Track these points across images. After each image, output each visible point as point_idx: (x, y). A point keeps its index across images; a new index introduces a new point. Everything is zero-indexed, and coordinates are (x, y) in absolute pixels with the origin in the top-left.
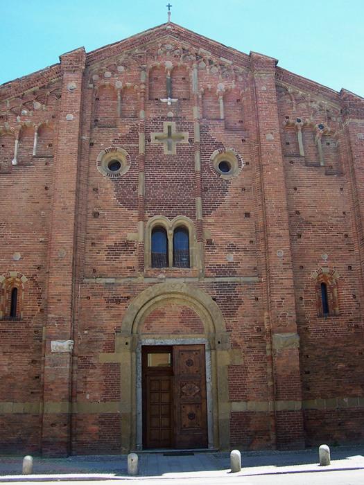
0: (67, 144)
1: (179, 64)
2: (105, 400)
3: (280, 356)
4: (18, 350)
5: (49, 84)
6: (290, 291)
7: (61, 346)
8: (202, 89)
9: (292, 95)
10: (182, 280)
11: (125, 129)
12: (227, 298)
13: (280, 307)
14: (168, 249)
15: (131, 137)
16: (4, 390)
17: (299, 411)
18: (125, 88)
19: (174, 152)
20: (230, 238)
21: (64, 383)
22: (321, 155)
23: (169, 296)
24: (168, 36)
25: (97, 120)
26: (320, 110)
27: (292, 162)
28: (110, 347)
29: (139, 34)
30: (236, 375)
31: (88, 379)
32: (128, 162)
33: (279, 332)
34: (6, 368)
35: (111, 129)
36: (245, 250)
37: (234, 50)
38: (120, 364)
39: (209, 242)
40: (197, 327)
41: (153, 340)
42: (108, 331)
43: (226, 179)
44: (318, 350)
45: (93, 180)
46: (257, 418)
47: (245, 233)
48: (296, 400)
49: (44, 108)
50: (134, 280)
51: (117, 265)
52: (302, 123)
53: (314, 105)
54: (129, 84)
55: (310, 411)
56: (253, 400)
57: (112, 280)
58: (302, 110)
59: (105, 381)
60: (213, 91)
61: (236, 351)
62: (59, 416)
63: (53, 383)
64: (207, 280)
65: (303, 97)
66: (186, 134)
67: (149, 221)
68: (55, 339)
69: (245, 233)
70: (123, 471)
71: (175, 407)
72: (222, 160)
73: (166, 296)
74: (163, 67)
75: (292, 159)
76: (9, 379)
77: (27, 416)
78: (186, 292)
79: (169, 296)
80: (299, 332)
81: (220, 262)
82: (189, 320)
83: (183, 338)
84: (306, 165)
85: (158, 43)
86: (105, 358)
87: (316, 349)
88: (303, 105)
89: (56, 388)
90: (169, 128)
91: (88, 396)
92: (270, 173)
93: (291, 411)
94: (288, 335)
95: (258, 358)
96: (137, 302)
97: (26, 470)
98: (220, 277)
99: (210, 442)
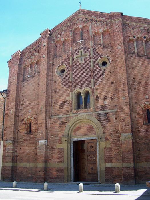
0: (43, 66)
1: (84, 25)
2: (58, 162)
3: (124, 143)
4: (31, 144)
5: (39, 45)
6: (128, 114)
7: (42, 142)
8: (94, 33)
9: (131, 26)
10: (86, 114)
11: (65, 56)
12: (104, 119)
13: (124, 122)
14: (82, 101)
15: (67, 59)
16: (27, 159)
17: (132, 167)
18: (65, 40)
19: (83, 62)
20: (105, 94)
21: (43, 156)
23: (82, 120)
24: (80, 15)
25: (56, 55)
26: (144, 30)
27: (131, 56)
28: (60, 142)
29: (69, 17)
30: (107, 151)
31: (53, 154)
32: (66, 69)
33: (123, 133)
34: (27, 151)
35: (60, 57)
36: (112, 98)
37: (105, 13)
38: (64, 148)
39: (97, 97)
40: (93, 132)
42: (59, 136)
43: (104, 69)
44: (144, 140)
45: (54, 78)
46: (116, 170)
47: (111, 91)
48: (131, 163)
49: (38, 54)
50: (68, 115)
52: (136, 38)
53: (142, 28)
54: (66, 38)
55: (140, 167)
56: (115, 162)
57: (61, 116)
58: (136, 32)
60: (98, 33)
61: (107, 142)
62: (42, 168)
63: (40, 156)
64: (96, 113)
65: (136, 26)
66: (87, 54)
67: (74, 91)
68: (40, 140)
69: (111, 91)
70: (42, 189)
71: (86, 165)
72: (60, 70)
73: (81, 121)
74: (78, 28)
75: (132, 55)
76: (28, 155)
77: (34, 168)
78: (87, 118)
79: (82, 120)
80: (133, 132)
81: (101, 105)
82: (90, 130)
83: (88, 137)
84: (138, 56)
85: (76, 19)
86: (58, 146)
87: (143, 139)
88: (137, 29)
91: (53, 161)
92: (119, 63)
93: (128, 168)
94: (127, 134)
95: (117, 144)
96: (70, 124)
97: (14, 186)
98: (101, 111)
99: (98, 180)
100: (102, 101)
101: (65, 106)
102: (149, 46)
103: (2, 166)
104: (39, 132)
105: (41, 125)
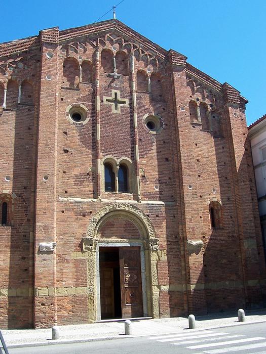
31: (64, 271)
51: (83, 189)
59: (76, 272)
63: (42, 273)
89: (44, 277)
90: (116, 94)
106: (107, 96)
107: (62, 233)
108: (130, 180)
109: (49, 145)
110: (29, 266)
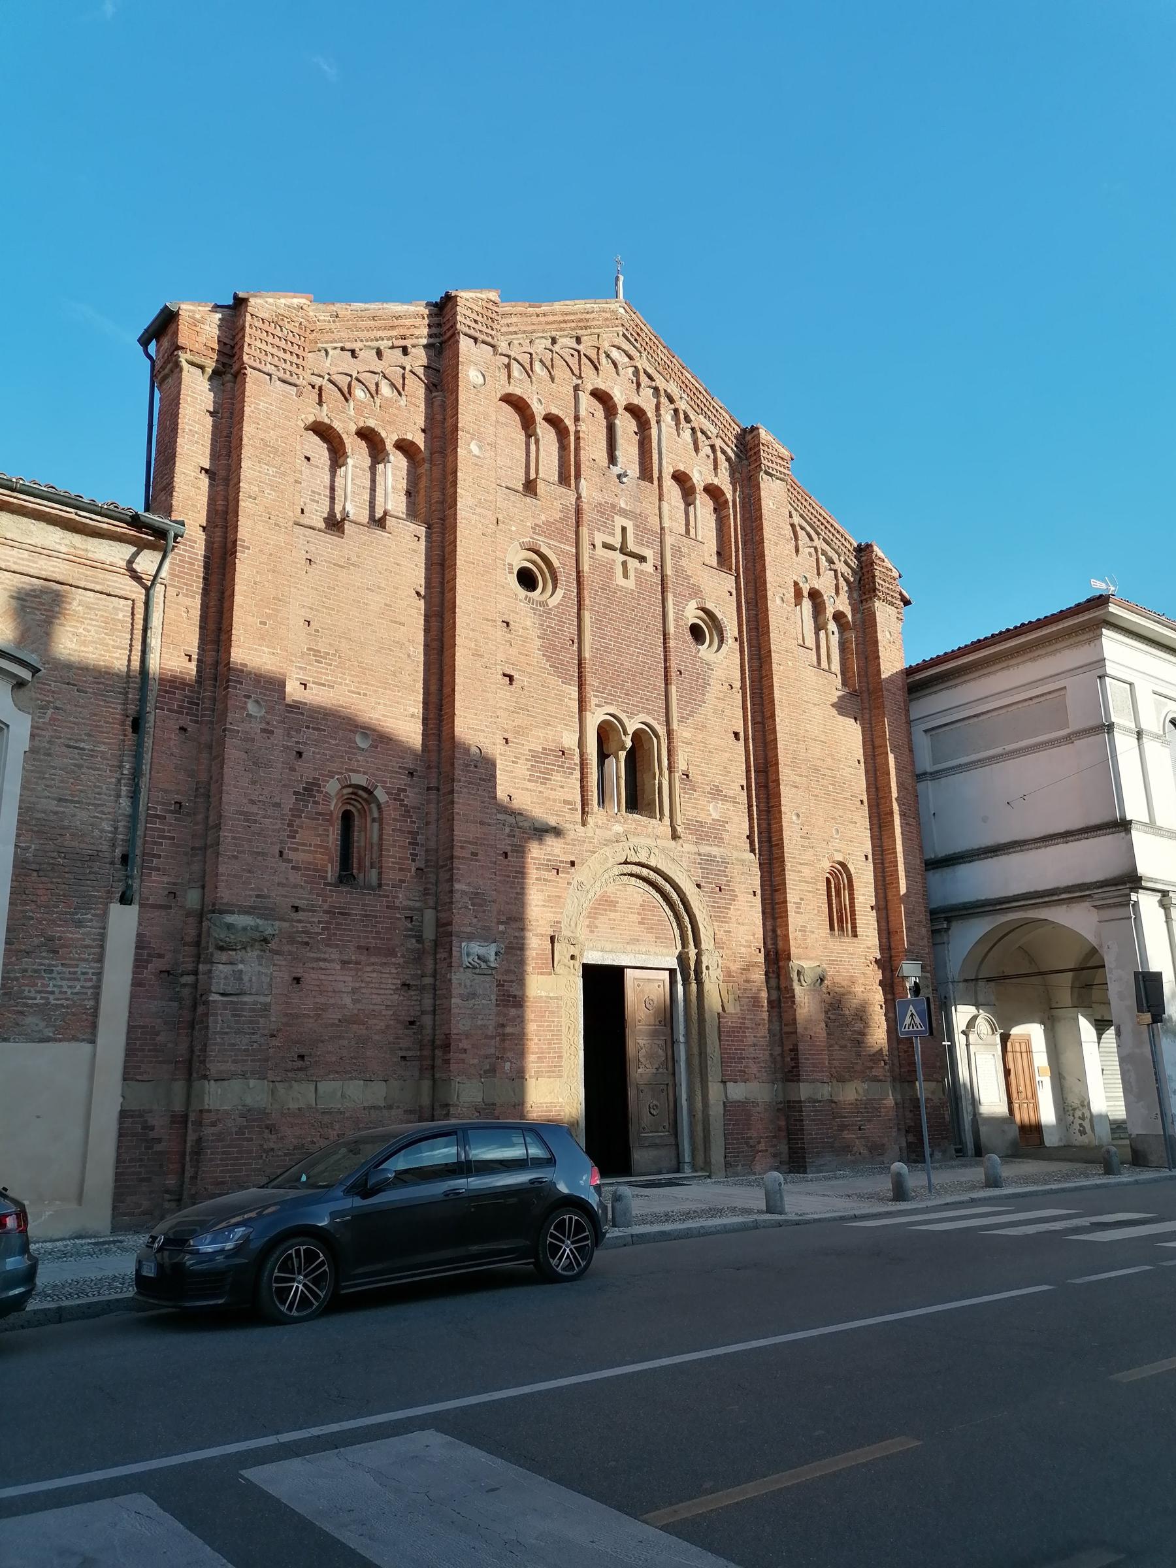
4: (373, 959)
22: (139, 842)
31: (508, 1030)
34: (347, 1000)
41: (600, 953)
51: (547, 793)
63: (468, 1036)
68: (470, 938)
100: (703, 801)
101: (557, 777)
102: (737, 644)
103: (123, 1115)
104: (464, 893)
105: (475, 854)
106: (604, 532)
107: (504, 919)
108: (639, 780)
109: (482, 656)
110: (423, 1013)
